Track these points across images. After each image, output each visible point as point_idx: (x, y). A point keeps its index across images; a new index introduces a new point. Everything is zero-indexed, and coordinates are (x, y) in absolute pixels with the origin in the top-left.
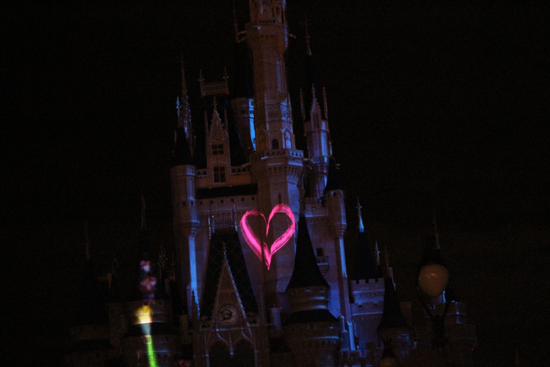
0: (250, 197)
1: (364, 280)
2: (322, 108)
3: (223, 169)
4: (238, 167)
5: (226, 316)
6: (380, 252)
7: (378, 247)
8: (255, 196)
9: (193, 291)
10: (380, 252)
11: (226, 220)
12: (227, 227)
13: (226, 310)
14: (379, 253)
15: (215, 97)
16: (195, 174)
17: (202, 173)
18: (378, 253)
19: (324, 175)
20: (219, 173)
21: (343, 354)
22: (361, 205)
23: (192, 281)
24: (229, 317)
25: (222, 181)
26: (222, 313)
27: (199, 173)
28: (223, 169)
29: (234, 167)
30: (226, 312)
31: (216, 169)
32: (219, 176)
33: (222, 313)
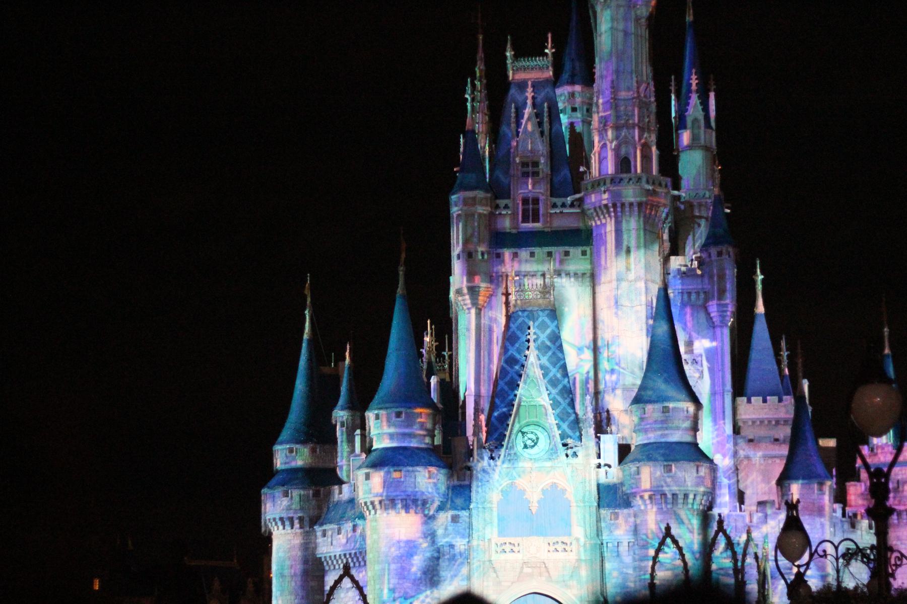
0: (580, 249)
1: (760, 398)
2: (706, 109)
3: (536, 201)
4: (563, 200)
5: (529, 443)
6: (789, 353)
7: (673, 138)
8: (588, 249)
9: (544, 377)
10: (789, 353)
11: (537, 285)
12: (531, 297)
13: (532, 433)
14: (787, 355)
15: (530, 83)
16: (491, 207)
17: (502, 205)
18: (786, 354)
19: (861, 447)
20: (531, 211)
21: (717, 518)
22: (762, 273)
23: (288, 421)
24: (533, 444)
25: (534, 221)
26: (523, 433)
27: (497, 207)
28: (536, 201)
29: (554, 200)
30: (530, 436)
31: (525, 201)
32: (531, 212)
33: (523, 433)
